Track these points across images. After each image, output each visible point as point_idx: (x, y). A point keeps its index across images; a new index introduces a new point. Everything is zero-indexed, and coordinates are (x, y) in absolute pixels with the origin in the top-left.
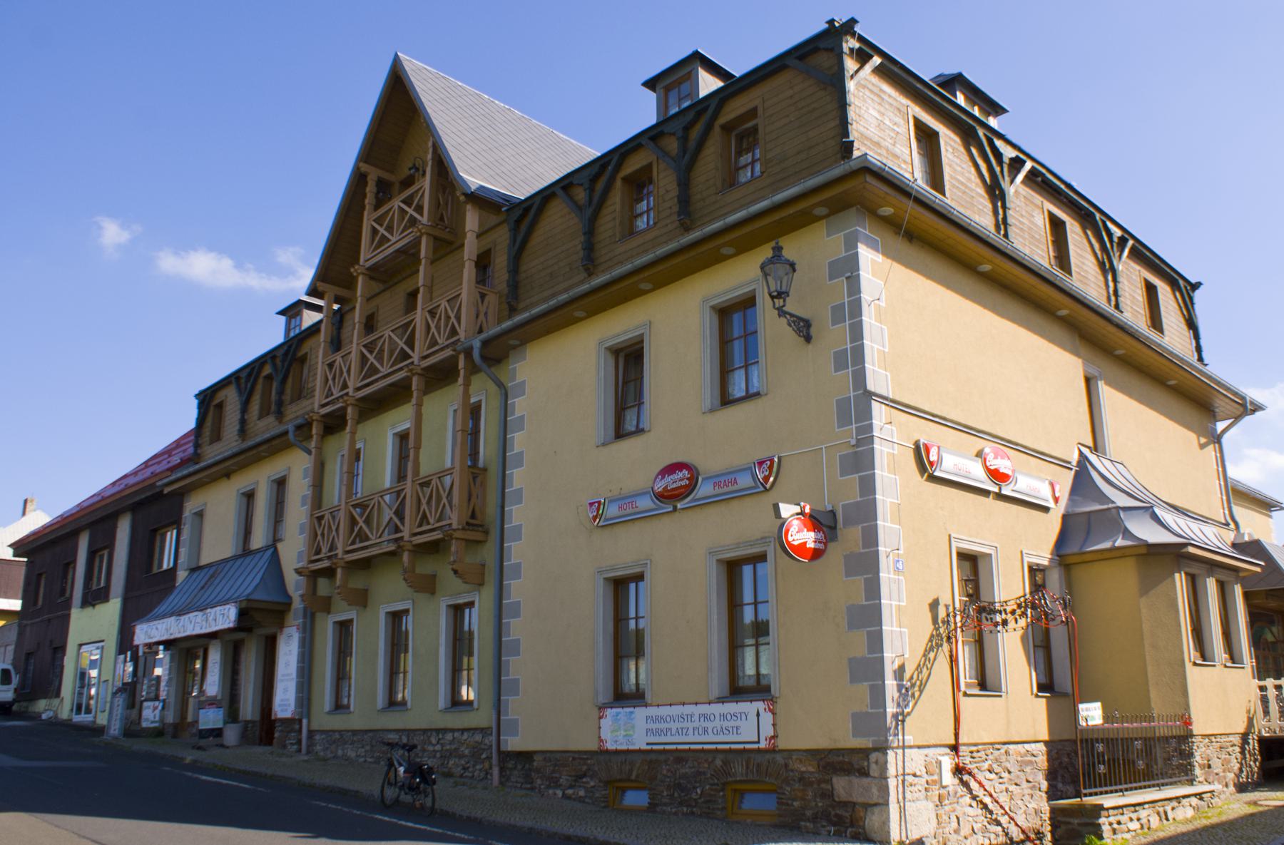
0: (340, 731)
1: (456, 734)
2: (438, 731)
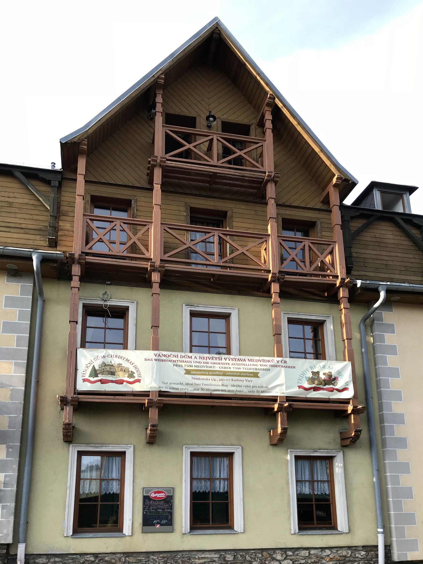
0: (96, 555)
1: (312, 552)
2: (284, 550)
